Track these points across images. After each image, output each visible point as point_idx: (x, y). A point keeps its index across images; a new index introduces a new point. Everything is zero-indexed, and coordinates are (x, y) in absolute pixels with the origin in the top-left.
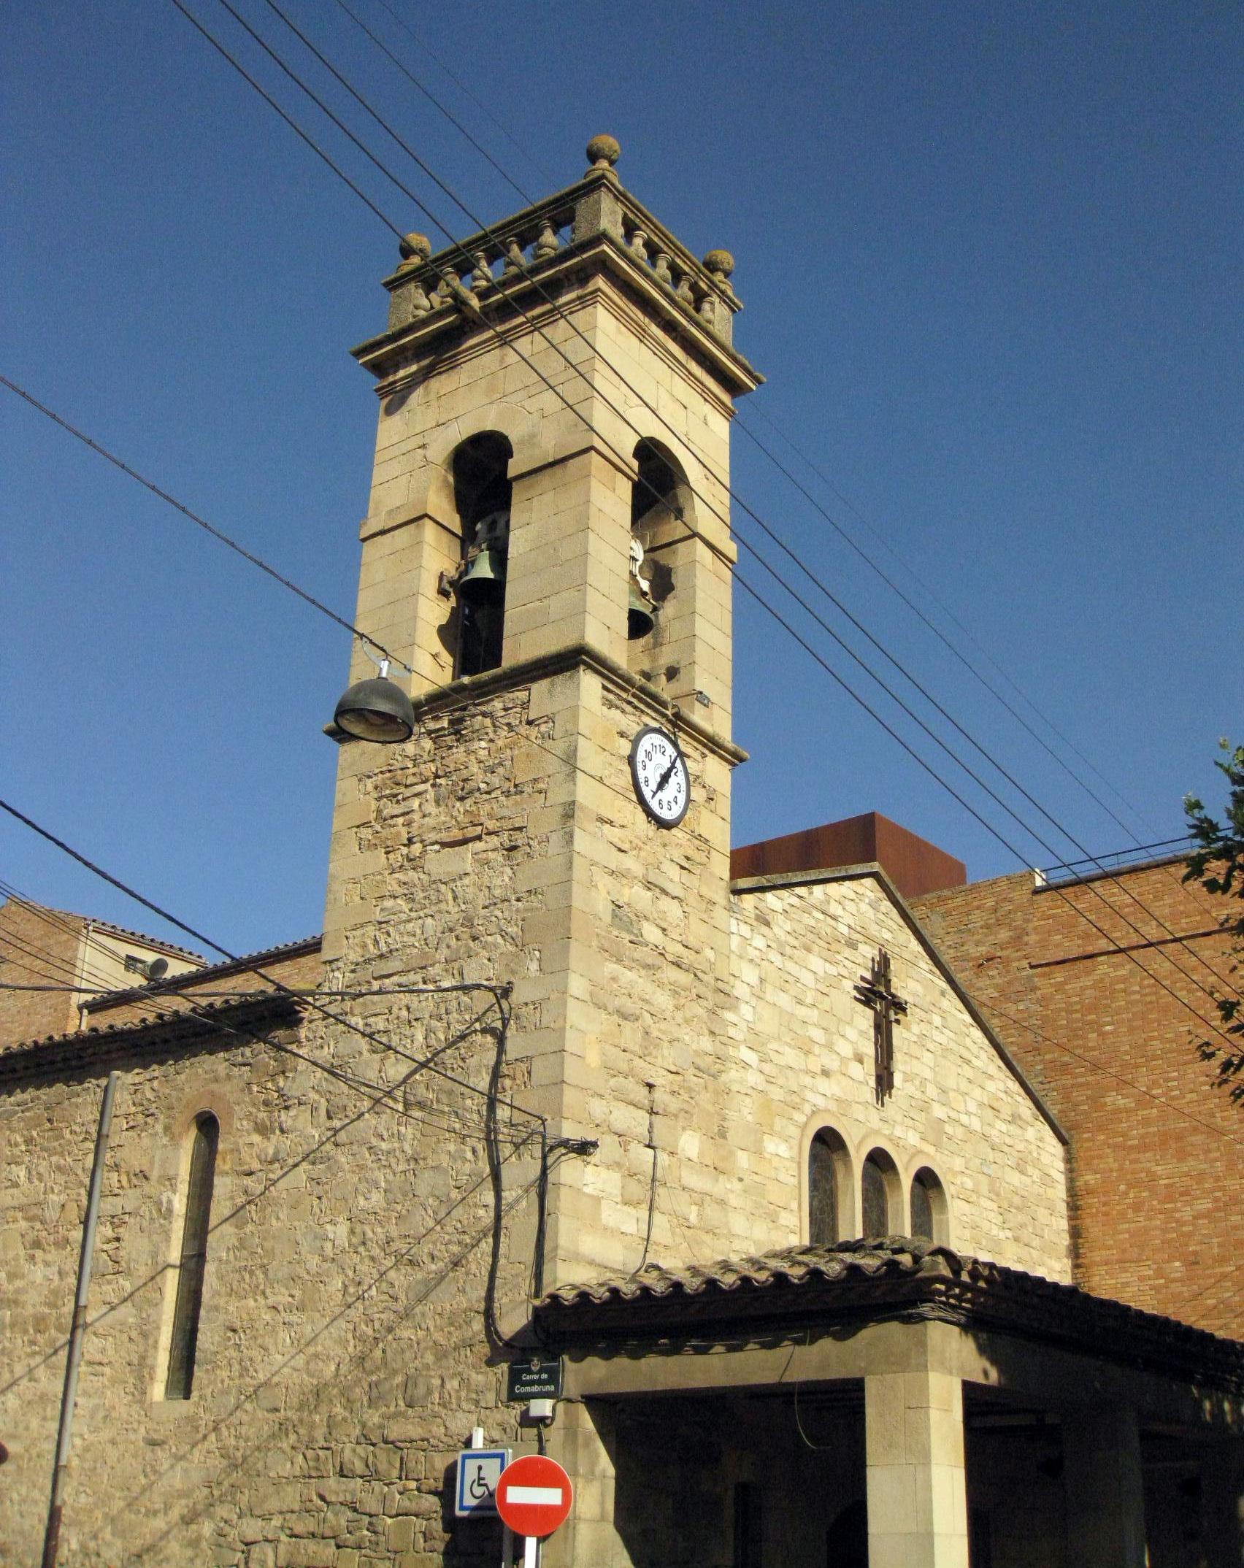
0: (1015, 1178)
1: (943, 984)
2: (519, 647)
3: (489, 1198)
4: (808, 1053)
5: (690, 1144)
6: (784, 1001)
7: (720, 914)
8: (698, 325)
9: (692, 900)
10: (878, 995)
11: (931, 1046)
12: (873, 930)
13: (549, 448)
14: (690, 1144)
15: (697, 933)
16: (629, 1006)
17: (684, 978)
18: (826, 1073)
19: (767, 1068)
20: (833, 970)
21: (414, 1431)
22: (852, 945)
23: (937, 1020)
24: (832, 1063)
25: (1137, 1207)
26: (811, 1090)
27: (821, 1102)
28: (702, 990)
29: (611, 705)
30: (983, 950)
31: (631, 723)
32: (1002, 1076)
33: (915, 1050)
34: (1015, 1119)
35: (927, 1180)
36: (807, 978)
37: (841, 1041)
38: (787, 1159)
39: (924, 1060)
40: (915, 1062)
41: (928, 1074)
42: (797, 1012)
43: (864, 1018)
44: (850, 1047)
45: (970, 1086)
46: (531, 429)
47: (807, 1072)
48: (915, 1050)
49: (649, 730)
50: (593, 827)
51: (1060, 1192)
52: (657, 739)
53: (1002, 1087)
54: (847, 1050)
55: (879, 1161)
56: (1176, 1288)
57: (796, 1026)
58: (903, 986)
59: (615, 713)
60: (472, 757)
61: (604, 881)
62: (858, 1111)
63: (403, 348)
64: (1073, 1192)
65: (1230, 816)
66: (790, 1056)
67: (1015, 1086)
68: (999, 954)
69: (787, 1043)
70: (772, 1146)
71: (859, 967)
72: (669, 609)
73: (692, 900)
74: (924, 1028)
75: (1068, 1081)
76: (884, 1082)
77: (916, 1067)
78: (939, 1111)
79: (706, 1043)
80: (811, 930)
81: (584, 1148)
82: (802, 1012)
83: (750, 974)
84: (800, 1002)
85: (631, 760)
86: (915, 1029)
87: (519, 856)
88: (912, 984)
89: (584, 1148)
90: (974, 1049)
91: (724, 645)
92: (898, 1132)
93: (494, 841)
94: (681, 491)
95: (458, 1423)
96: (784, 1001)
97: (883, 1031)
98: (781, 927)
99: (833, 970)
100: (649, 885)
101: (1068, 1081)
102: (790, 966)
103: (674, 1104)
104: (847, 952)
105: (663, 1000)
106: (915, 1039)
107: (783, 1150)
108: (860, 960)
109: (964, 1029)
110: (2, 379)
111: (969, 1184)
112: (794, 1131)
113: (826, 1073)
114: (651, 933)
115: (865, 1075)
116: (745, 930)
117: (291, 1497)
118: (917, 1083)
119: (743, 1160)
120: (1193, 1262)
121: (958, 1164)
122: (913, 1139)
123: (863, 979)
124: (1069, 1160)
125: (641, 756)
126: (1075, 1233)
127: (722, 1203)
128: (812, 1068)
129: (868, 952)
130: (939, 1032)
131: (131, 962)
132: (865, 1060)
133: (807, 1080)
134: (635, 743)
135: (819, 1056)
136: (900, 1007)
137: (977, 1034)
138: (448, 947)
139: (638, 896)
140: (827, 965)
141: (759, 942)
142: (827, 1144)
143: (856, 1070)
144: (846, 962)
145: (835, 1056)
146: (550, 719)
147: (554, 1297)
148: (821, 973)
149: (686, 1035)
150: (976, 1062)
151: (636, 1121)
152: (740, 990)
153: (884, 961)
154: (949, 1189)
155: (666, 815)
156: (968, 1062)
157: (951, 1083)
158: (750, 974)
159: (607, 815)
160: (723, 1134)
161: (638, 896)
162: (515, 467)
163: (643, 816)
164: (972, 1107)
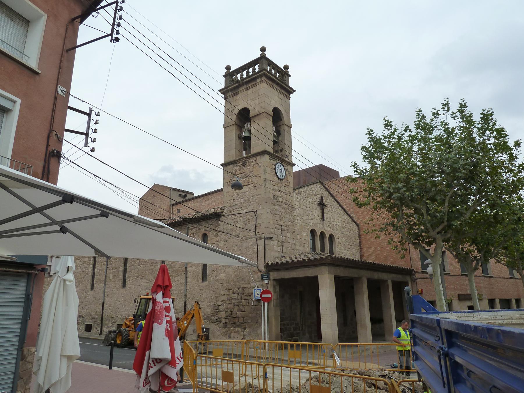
0: (348, 233)
1: (333, 200)
2: (255, 150)
3: (256, 247)
5: (289, 235)
6: (304, 207)
7: (292, 194)
8: (283, 83)
9: (287, 192)
10: (322, 205)
12: (320, 192)
13: (256, 112)
14: (289, 235)
15: (288, 197)
16: (277, 213)
17: (286, 206)
18: (312, 219)
19: (302, 220)
21: (245, 286)
22: (316, 195)
23: (333, 207)
25: (371, 238)
27: (311, 224)
28: (290, 208)
29: (271, 160)
31: (274, 162)
34: (348, 223)
35: (331, 237)
38: (306, 235)
43: (319, 209)
46: (254, 108)
48: (329, 213)
49: (277, 163)
50: (269, 182)
51: (357, 235)
52: (279, 164)
55: (322, 234)
56: (378, 252)
58: (326, 201)
59: (272, 161)
60: (248, 169)
61: (271, 191)
62: (318, 225)
63: (228, 90)
64: (359, 235)
65: (335, 257)
66: (306, 217)
67: (347, 217)
70: (303, 233)
71: (317, 200)
72: (280, 138)
73: (287, 192)
74: (330, 208)
75: (358, 214)
76: (323, 219)
78: (333, 223)
79: (291, 217)
80: (308, 194)
81: (271, 238)
82: (307, 209)
83: (298, 204)
84: (307, 207)
85: (275, 169)
87: (256, 188)
88: (327, 201)
89: (271, 238)
91: (292, 276)
92: (326, 228)
93: (252, 185)
94: (281, 123)
95: (252, 284)
96: (304, 207)
97: (322, 210)
98: (303, 194)
100: (279, 191)
101: (358, 214)
103: (286, 228)
104: (315, 197)
105: (283, 210)
107: (305, 234)
111: (339, 235)
112: (307, 230)
113: (312, 219)
114: (280, 199)
115: (319, 218)
116: (297, 196)
117: (225, 297)
119: (298, 236)
120: (382, 248)
121: (337, 232)
122: (329, 229)
124: (359, 229)
125: (277, 168)
126: (360, 242)
127: (295, 244)
129: (319, 196)
130: (333, 211)
131: (180, 195)
134: (275, 166)
137: (340, 208)
139: (278, 193)
141: (299, 198)
142: (313, 232)
143: (318, 218)
146: (261, 163)
147: (267, 264)
149: (287, 216)
151: (278, 232)
152: (296, 207)
153: (322, 198)
154: (335, 237)
155: (281, 178)
158: (298, 204)
159: (271, 180)
160: (294, 232)
161: (278, 193)
162: (251, 115)
163: (277, 179)
164: (340, 222)
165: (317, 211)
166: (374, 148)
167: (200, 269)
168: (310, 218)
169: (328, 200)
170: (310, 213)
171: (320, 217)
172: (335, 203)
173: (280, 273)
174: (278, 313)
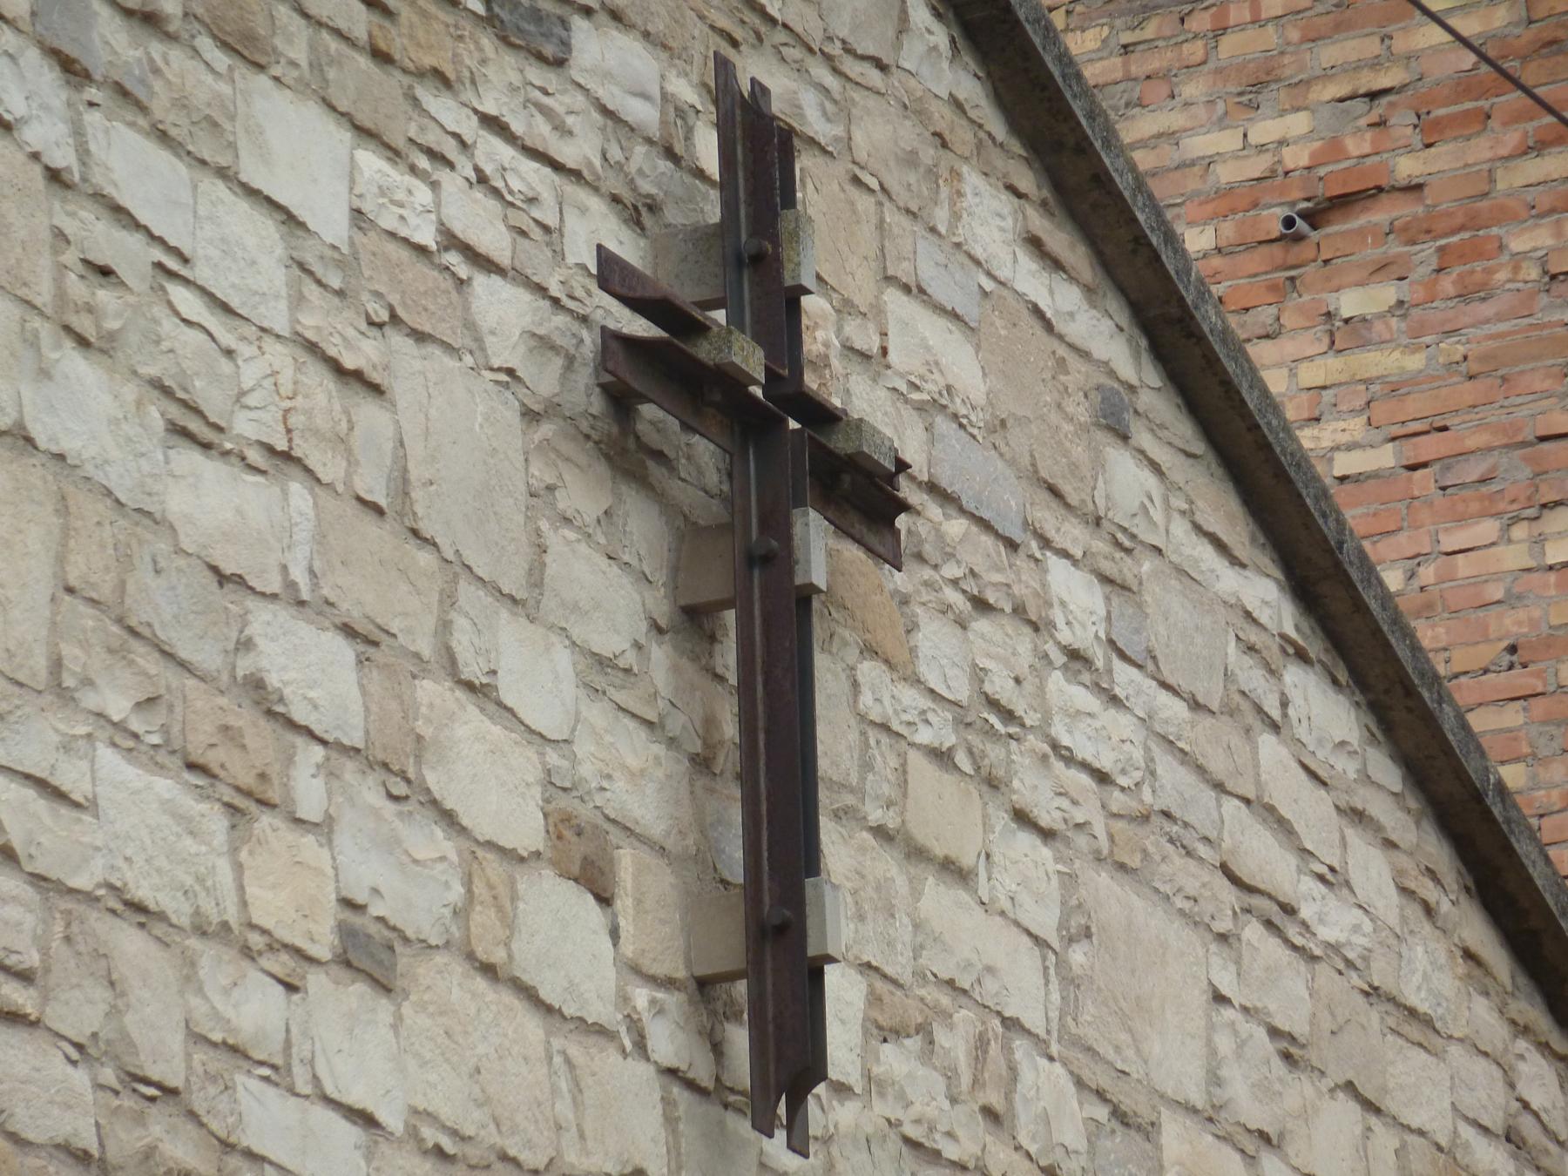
1: (1104, 336)
4: (250, 802)
10: (730, 427)
11: (1034, 787)
18: (369, 954)
20: (416, 209)
23: (1076, 599)
24: (415, 885)
26: (277, 1074)
30: (1289, 133)
32: (1483, 1017)
33: (945, 811)
36: (238, 252)
37: (471, 725)
39: (1001, 884)
40: (938, 898)
41: (1026, 992)
42: (176, 502)
43: (606, 580)
44: (526, 764)
45: (1299, 1090)
47: (249, 943)
48: (945, 811)
53: (1490, 1102)
54: (498, 792)
57: (164, 602)
68: (1407, 167)
69: (123, 736)
74: (1000, 649)
77: (961, 931)
82: (212, 502)
84: (193, 430)
86: (937, 647)
88: (917, 337)
90: (1311, 811)
97: (757, 652)
99: (416, 209)
102: (128, 161)
106: (939, 731)
108: (579, 150)
109: (1252, 677)
110: (1, 287)
113: (369, 954)
118: (955, 1042)
123: (610, 272)
128: (273, 907)
132: (627, 862)
133: (255, 1009)
135: (324, 828)
136: (868, 496)
137: (1325, 713)
138: (293, 64)
140: (371, 162)
143: (566, 941)
144: (493, 152)
145: (430, 841)
148: (329, 223)
150: (1332, 920)
153: (762, 152)
156: (1281, 915)
157: (1173, 1059)
165: (539, 679)
166: (861, 420)
167: (223, 424)
168: (289, 890)
169: (938, 311)
170: (312, 669)
171: (656, 915)
172: (1154, 482)
173: (736, 755)
174: (1124, 318)
